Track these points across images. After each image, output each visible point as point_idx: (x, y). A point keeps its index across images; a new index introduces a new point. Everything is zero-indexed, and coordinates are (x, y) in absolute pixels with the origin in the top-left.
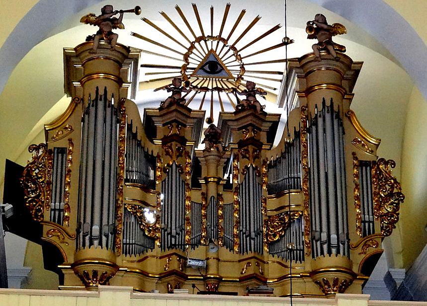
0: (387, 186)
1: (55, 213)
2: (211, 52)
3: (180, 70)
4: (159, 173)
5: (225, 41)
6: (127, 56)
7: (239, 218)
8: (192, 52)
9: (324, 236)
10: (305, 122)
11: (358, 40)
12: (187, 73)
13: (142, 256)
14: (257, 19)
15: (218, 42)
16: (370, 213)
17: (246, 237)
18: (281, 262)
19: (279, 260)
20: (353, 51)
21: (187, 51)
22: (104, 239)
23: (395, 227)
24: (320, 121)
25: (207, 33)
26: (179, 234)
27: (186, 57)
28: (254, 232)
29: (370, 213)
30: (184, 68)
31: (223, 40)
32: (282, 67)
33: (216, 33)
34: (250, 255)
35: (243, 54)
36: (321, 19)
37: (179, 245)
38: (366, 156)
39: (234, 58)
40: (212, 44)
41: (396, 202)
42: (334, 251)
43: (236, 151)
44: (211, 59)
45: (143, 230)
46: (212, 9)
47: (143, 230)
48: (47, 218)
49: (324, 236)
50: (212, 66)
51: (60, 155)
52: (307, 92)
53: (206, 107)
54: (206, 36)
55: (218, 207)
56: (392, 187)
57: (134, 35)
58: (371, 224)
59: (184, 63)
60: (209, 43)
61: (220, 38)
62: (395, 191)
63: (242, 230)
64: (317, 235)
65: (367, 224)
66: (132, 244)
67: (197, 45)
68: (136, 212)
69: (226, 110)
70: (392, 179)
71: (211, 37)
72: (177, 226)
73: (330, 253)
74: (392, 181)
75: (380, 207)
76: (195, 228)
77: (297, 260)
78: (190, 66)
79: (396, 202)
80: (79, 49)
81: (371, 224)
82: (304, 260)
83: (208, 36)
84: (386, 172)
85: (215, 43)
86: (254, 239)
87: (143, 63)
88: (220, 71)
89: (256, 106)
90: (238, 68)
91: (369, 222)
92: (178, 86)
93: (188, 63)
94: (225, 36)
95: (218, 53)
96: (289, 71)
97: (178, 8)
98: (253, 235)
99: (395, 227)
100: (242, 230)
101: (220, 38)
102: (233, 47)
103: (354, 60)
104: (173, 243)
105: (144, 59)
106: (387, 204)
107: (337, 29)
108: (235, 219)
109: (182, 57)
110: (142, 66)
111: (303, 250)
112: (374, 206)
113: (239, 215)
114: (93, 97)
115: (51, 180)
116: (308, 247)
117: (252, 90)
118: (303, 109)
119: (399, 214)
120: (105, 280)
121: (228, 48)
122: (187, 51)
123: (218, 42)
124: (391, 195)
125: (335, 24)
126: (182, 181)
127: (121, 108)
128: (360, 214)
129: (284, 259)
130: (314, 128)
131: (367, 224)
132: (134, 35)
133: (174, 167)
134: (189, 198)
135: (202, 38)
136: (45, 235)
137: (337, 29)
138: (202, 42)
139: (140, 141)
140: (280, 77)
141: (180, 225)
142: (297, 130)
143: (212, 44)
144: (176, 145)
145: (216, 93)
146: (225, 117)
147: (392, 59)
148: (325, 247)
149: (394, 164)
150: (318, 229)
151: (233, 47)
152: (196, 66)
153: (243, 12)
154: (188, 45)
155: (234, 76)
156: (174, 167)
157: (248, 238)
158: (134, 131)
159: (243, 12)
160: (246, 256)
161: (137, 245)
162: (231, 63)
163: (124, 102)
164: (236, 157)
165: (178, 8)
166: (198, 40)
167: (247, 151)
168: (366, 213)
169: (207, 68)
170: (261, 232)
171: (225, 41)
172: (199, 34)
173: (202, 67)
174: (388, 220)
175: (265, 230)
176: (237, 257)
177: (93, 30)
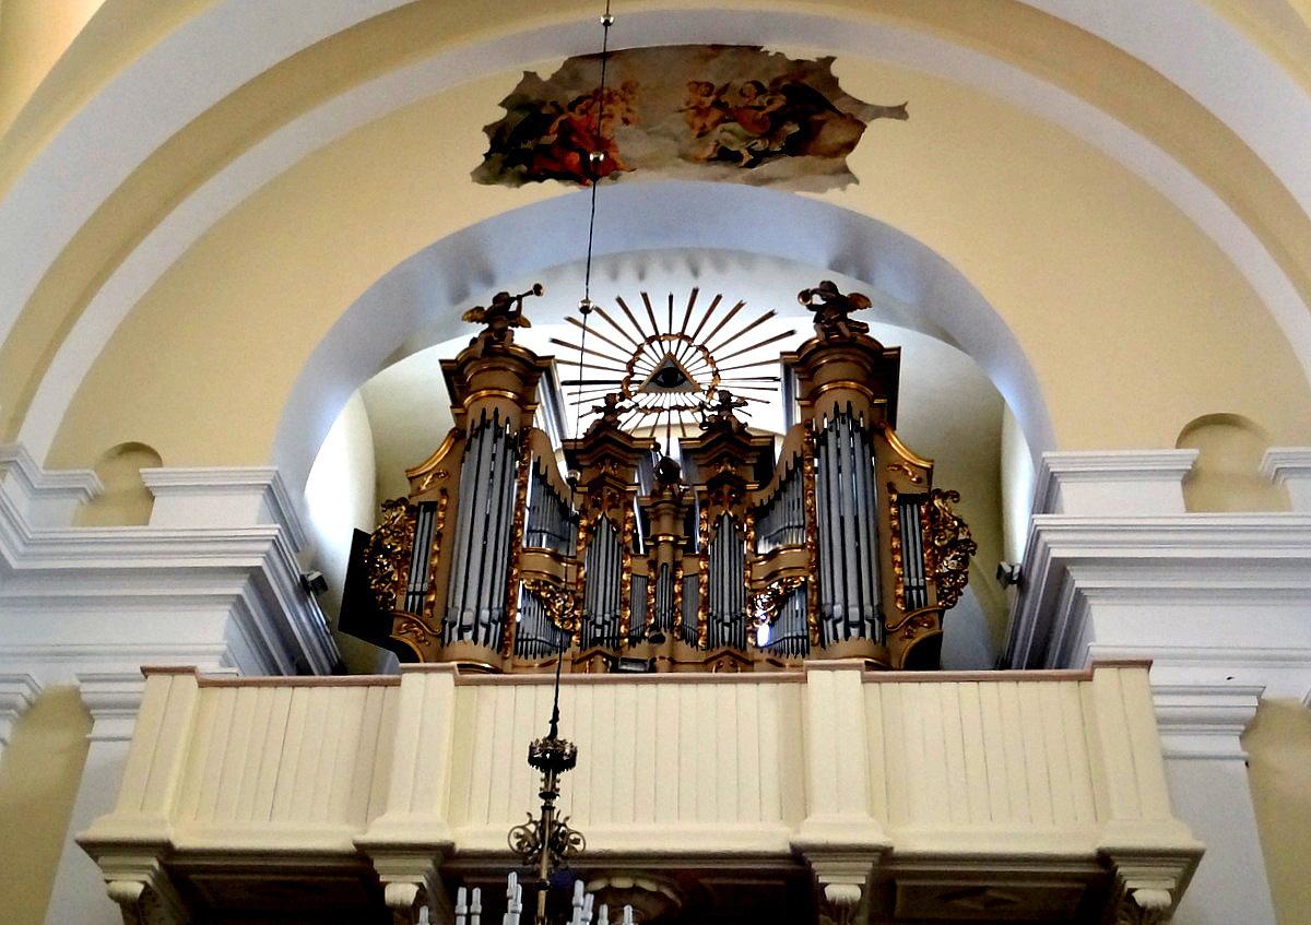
0: (946, 531)
1: (414, 599)
2: (670, 357)
3: (619, 386)
4: (581, 535)
5: (690, 340)
6: (535, 369)
7: (708, 595)
8: (639, 359)
9: (838, 610)
10: (808, 443)
11: (892, 317)
12: (630, 389)
13: (547, 659)
14: (740, 305)
15: (680, 342)
16: (920, 575)
17: (717, 623)
18: (775, 658)
19: (769, 657)
20: (883, 333)
21: (631, 357)
22: (482, 631)
23: (961, 594)
24: (831, 436)
25: (663, 329)
26: (609, 623)
27: (631, 365)
28: (730, 614)
29: (920, 575)
30: (628, 381)
31: (687, 338)
32: (776, 370)
33: (676, 329)
34: (722, 649)
35: (716, 356)
36: (828, 289)
37: (608, 638)
38: (906, 487)
39: (704, 362)
40: (671, 346)
41: (963, 554)
42: (854, 631)
43: (704, 496)
44: (669, 365)
45: (551, 619)
46: (671, 298)
47: (551, 619)
48: (400, 606)
49: (838, 610)
50: (670, 377)
51: (428, 514)
52: (812, 397)
53: (661, 438)
54: (661, 334)
55: (674, 579)
56: (956, 531)
57: (554, 341)
58: (922, 592)
59: (628, 374)
60: (666, 344)
61: (682, 336)
62: (961, 537)
63: (712, 614)
64: (827, 610)
65: (914, 592)
66: (532, 640)
67: (646, 348)
68: (540, 591)
69: (689, 435)
70: (955, 518)
71: (669, 336)
72: (607, 610)
73: (847, 634)
74: (956, 523)
75: (936, 563)
76: (638, 614)
77: (797, 653)
78: (636, 378)
79: (963, 554)
80: (468, 357)
81: (922, 592)
82: (808, 653)
83: (664, 335)
84: (944, 510)
85: (675, 343)
86: (729, 625)
87: (561, 380)
88: (682, 382)
89: (730, 423)
90: (711, 377)
91: (918, 588)
92: (611, 408)
93: (633, 374)
94: (690, 332)
95: (678, 358)
96: (787, 369)
97: (620, 301)
98: (727, 619)
99: (961, 594)
100: (712, 614)
101: (682, 336)
102: (702, 348)
103: (885, 346)
104: (598, 635)
105: (563, 373)
106: (948, 558)
107: (858, 301)
108: (701, 598)
109: (624, 367)
110: (564, 383)
111: (807, 637)
112: (926, 562)
113: (708, 592)
114: (477, 424)
115: (411, 547)
116: (815, 632)
117: (727, 402)
118: (807, 424)
119: (967, 573)
120: (126, 491)
121: (695, 349)
122: (631, 357)
123: (680, 342)
124: (954, 544)
125: (852, 295)
126: (619, 545)
127: (522, 441)
128: (900, 576)
129: (778, 655)
130: (823, 449)
131: (914, 592)
132: (554, 341)
133: (605, 522)
134: (628, 570)
135: (656, 337)
136: (394, 631)
137: (858, 301)
138: (656, 344)
139: (553, 487)
140: (778, 385)
141: (613, 608)
142: (799, 455)
143: (671, 346)
144: (609, 491)
145: (674, 413)
146: (690, 445)
147: (948, 338)
148: (840, 626)
149: (958, 495)
150: (829, 601)
151: (702, 348)
152: (644, 378)
153: (719, 298)
154: (634, 349)
155: (702, 387)
156: (605, 522)
157: (720, 625)
158: (542, 472)
159: (719, 298)
160: (716, 652)
161: (540, 641)
162: (701, 373)
163: (528, 431)
164: (704, 505)
165: (620, 301)
166: (650, 340)
167: (720, 494)
168: (913, 574)
169: (660, 379)
170: (742, 614)
171: (690, 340)
172: (650, 332)
173: (654, 379)
174: (950, 583)
175: (749, 611)
176: (703, 657)
177: (477, 329)
